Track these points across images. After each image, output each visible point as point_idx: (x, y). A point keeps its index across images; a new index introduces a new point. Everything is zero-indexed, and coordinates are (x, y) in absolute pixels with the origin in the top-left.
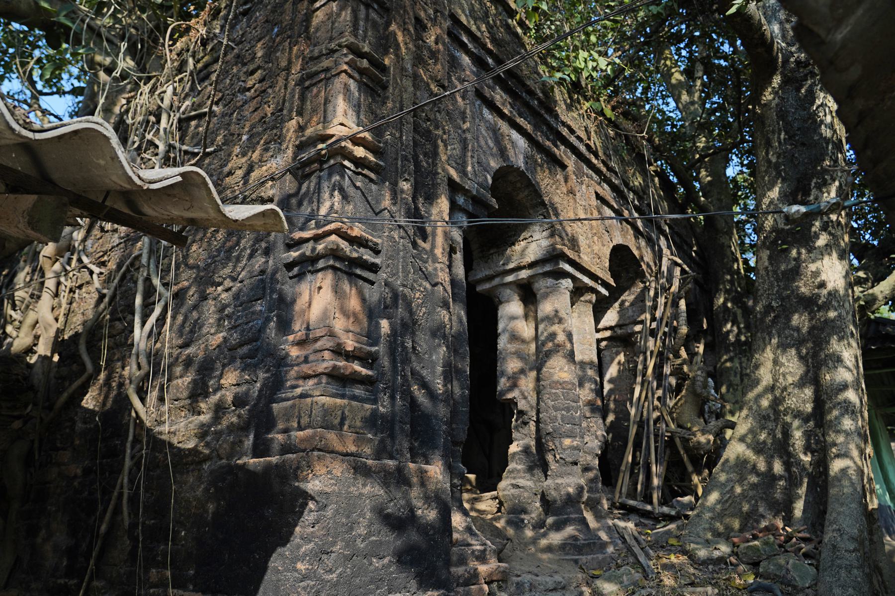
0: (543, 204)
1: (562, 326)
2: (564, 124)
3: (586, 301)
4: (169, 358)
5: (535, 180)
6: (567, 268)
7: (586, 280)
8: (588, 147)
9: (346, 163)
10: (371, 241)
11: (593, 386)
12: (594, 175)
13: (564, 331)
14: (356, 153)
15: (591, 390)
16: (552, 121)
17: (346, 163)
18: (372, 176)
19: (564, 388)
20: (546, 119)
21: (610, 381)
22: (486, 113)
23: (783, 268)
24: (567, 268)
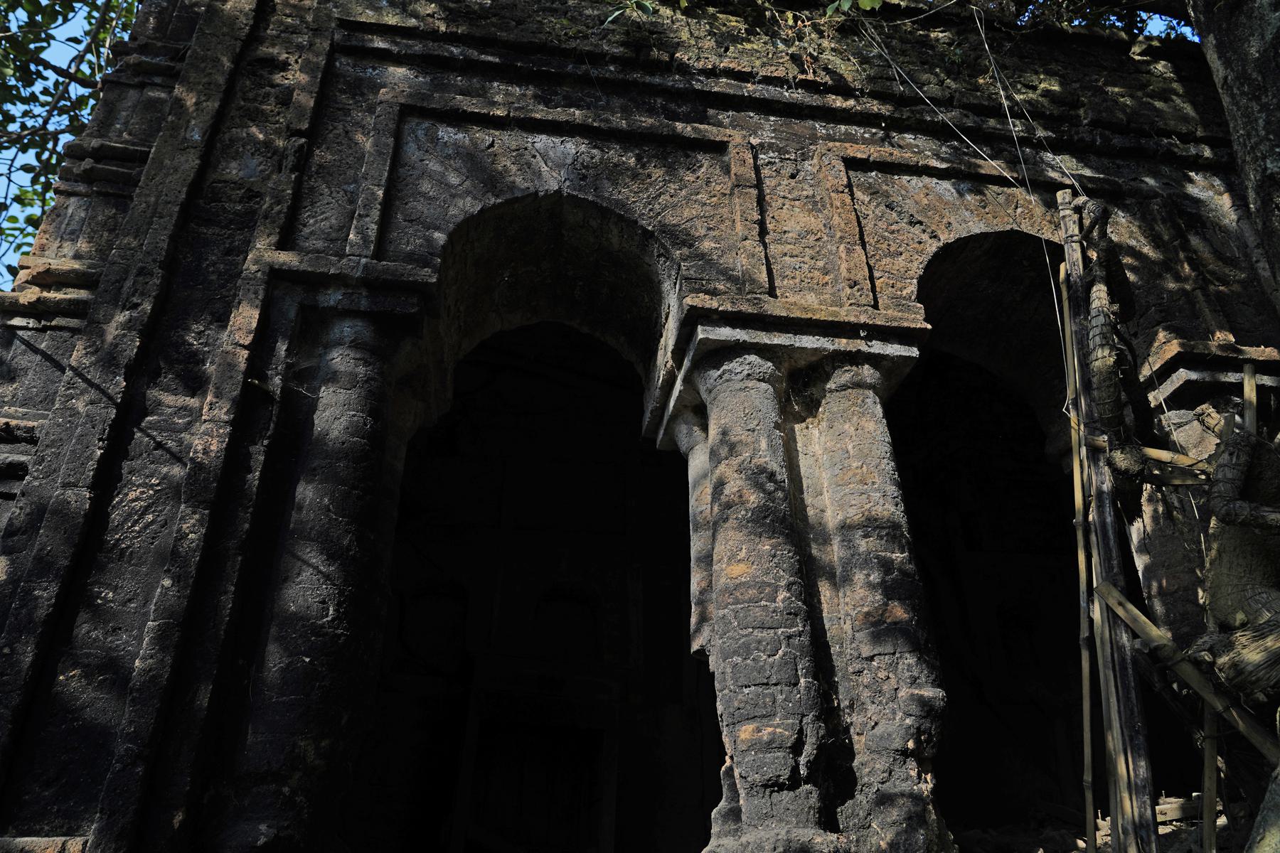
0: (647, 235)
1: (735, 462)
2: (713, 73)
3: (844, 388)
4: (920, 686)
5: (603, 198)
6: (725, 333)
7: (809, 342)
8: (805, 85)
9: (17, 321)
10: (18, 428)
11: (875, 577)
12: (853, 129)
13: (739, 471)
14: (22, 301)
15: (871, 586)
16: (675, 81)
17: (17, 321)
18: (74, 323)
19: (737, 602)
20: (651, 85)
21: (1143, 548)
22: (447, 134)
23: (1254, 51)
24: (725, 333)
